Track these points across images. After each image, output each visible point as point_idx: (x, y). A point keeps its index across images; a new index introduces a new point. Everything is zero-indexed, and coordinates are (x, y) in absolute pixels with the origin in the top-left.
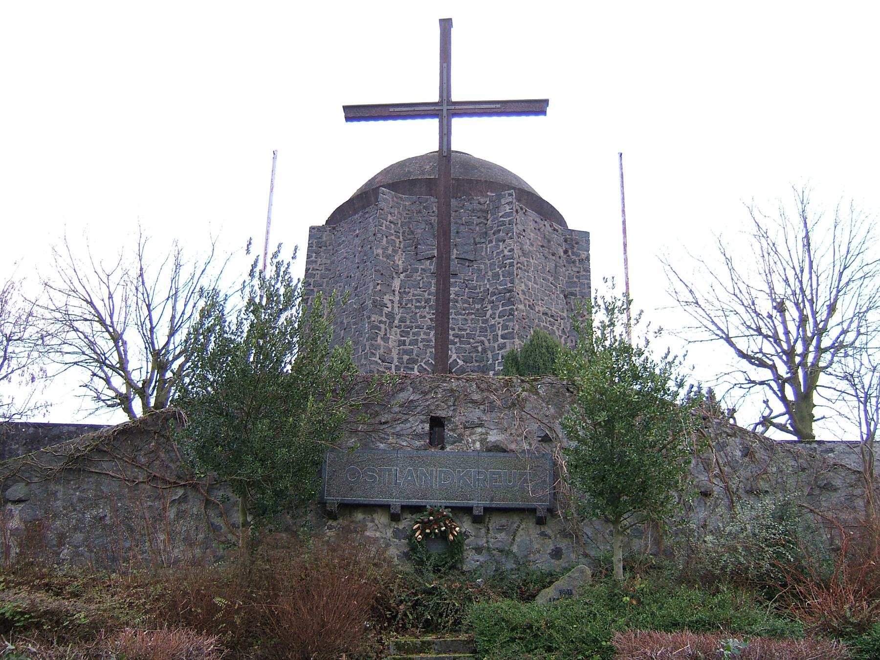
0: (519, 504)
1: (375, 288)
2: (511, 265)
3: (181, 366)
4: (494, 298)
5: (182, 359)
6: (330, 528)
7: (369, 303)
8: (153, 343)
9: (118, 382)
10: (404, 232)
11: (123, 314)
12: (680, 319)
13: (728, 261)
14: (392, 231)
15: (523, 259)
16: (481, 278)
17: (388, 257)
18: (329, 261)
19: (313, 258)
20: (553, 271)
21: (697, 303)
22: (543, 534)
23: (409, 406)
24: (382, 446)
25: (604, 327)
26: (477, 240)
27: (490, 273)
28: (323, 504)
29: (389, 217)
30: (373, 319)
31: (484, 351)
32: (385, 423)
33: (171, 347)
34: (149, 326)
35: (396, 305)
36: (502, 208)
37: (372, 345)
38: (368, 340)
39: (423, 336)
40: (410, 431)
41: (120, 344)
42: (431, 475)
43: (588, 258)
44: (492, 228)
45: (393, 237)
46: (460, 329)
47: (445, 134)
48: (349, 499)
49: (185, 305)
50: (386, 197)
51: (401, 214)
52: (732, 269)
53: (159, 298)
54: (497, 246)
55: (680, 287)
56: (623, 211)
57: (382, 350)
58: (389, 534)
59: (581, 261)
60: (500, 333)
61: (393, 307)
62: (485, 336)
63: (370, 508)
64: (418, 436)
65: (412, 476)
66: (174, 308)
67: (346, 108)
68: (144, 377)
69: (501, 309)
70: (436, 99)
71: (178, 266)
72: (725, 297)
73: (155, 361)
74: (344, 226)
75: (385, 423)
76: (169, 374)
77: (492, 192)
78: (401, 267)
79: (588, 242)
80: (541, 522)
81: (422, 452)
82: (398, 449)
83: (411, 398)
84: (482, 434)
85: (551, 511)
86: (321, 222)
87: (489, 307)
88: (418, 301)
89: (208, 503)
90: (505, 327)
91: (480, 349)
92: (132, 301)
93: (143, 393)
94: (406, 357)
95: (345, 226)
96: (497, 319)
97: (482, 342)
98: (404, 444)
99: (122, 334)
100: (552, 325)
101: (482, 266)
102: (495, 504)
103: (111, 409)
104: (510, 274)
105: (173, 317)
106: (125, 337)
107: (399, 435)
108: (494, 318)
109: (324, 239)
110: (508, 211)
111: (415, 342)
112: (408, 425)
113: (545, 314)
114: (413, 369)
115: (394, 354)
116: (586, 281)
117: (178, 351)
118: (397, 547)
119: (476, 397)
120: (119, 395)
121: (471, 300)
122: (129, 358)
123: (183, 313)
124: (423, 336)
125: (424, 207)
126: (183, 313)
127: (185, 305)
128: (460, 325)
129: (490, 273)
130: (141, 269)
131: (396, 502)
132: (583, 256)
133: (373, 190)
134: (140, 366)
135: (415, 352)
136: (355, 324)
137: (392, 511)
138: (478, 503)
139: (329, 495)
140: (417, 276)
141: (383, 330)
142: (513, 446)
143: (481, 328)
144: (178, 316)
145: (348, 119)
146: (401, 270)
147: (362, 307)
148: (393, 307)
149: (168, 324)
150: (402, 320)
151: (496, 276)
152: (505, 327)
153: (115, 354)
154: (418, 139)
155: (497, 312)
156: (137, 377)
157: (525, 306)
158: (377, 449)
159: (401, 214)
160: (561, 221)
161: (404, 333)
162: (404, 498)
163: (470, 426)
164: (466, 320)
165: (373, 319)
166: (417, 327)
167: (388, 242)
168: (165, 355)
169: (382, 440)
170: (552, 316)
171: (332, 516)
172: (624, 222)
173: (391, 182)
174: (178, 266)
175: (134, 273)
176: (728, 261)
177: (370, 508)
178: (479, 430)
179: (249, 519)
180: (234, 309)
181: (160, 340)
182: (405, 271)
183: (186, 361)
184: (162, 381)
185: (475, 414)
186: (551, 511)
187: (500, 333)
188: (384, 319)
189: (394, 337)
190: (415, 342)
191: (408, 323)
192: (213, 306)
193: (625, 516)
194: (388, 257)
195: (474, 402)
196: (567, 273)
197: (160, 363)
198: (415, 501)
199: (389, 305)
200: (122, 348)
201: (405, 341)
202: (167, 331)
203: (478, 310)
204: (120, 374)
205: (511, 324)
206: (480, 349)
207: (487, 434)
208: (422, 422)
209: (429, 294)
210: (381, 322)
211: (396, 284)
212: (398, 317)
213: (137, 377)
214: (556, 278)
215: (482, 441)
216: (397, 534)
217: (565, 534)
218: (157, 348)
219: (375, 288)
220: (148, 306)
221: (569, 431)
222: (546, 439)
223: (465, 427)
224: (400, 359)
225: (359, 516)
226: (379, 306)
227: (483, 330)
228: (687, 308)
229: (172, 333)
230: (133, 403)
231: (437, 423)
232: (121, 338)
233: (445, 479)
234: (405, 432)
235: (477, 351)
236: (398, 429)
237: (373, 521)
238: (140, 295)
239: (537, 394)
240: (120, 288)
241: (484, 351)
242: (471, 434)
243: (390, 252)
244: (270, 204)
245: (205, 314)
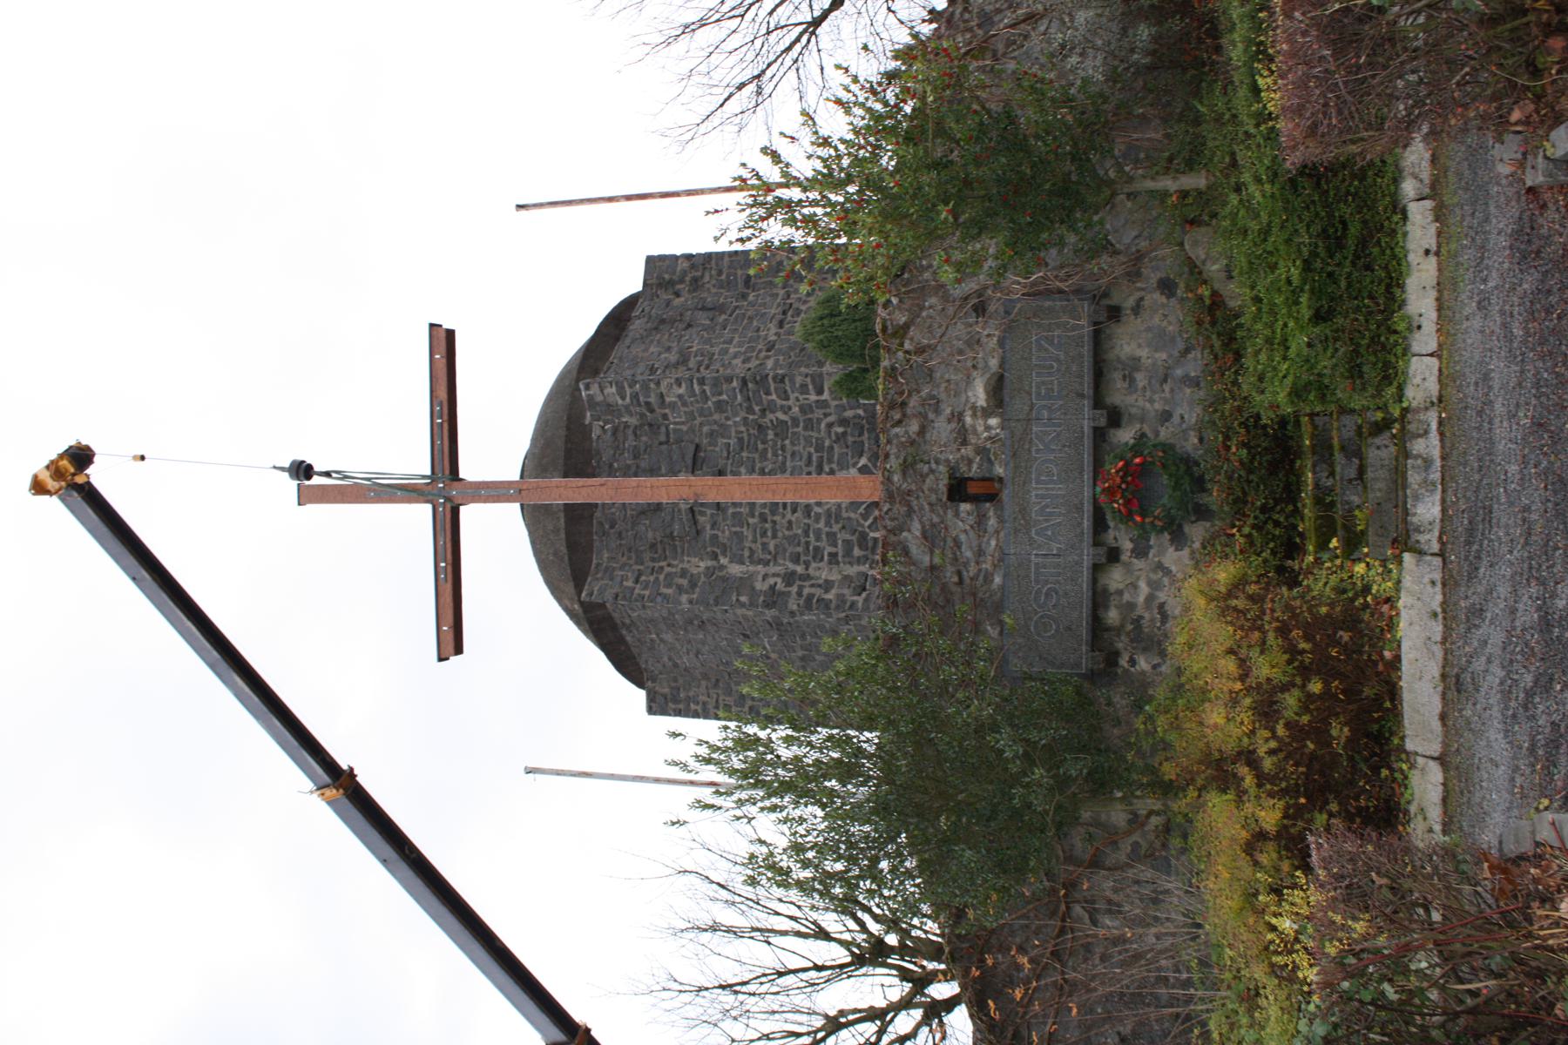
0: (1086, 350)
1: (743, 605)
2: (702, 382)
3: (876, 918)
4: (757, 409)
5: (866, 918)
6: (1133, 662)
7: (770, 614)
8: (842, 966)
9: (904, 1022)
10: (653, 560)
11: (798, 1017)
12: (783, 110)
13: (688, 29)
14: (652, 578)
15: (692, 364)
16: (723, 430)
17: (693, 585)
18: (704, 683)
19: (699, 708)
20: (710, 314)
21: (758, 77)
22: (1137, 309)
23: (931, 537)
24: (998, 580)
25: (791, 222)
26: (663, 438)
27: (716, 417)
28: (1092, 676)
29: (629, 584)
30: (795, 607)
31: (843, 422)
32: (959, 573)
33: (847, 937)
34: (813, 974)
35: (772, 569)
36: (610, 400)
37: (838, 607)
38: (829, 615)
39: (821, 525)
40: (972, 534)
41: (843, 1020)
42: (1043, 497)
43: (689, 257)
44: (642, 415)
45: (662, 577)
46: (809, 463)
47: (492, 492)
48: (1084, 632)
49: (777, 913)
50: (596, 589)
51: (624, 565)
52: (703, 23)
53: (762, 956)
54: (673, 406)
55: (733, 106)
56: (610, 199)
57: (846, 591)
58: (1138, 564)
59: (693, 267)
60: (813, 397)
61: (774, 575)
62: (819, 421)
63: (1099, 598)
64: (981, 520)
65: (1046, 529)
66: (784, 933)
67: (441, 659)
68: (896, 981)
69: (774, 397)
70: (427, 509)
71: (714, 928)
72: (747, 28)
73: (875, 963)
74: (646, 661)
75: (959, 573)
76: (892, 940)
77: (584, 417)
78: (710, 563)
79: (662, 258)
80: (1115, 313)
81: (1007, 513)
82: (1003, 556)
83: (918, 533)
84: (974, 415)
85: (1098, 297)
86: (641, 694)
87: (771, 416)
88: (764, 534)
89: (1095, 863)
90: (804, 389)
91: (840, 430)
92: (772, 1003)
93: (921, 982)
94: (857, 552)
95: (644, 656)
96: (790, 403)
97: (830, 425)
98: (993, 543)
99: (826, 1016)
100: (798, 312)
101: (705, 429)
102: (1087, 389)
103: (949, 1031)
104: (716, 383)
105: (798, 934)
106: (832, 1013)
107: (980, 553)
108: (790, 408)
109: (666, 690)
110: (614, 390)
111: (832, 538)
112: (963, 537)
113: (781, 324)
114: (875, 540)
115: (852, 570)
116: (726, 259)
117: (852, 925)
118: (1162, 552)
119: (914, 427)
120: (926, 1020)
121: (760, 446)
122: (865, 1006)
123: (791, 918)
124: (821, 525)
125: (612, 527)
126: (791, 918)
127: (777, 913)
128: (802, 463)
129: (716, 417)
130: (722, 987)
131: (1087, 556)
132: (686, 265)
133: (585, 612)
134: (878, 987)
135: (848, 537)
136: (803, 636)
137: (1104, 560)
138: (1087, 419)
139: (1078, 665)
140: (724, 536)
141: (813, 590)
142: (994, 363)
143: (805, 428)
144: (798, 927)
145: (459, 650)
146: (714, 563)
147: (776, 625)
148: (774, 575)
149: (810, 941)
150: (796, 559)
151: (720, 406)
152: (804, 389)
153: (860, 1027)
154: (498, 540)
155: (779, 402)
156: (898, 990)
157: (768, 357)
158: (1002, 587)
159: (624, 565)
160: (629, 304)
161: (817, 554)
162: (1081, 541)
163: (962, 436)
164: (793, 454)
165: (795, 607)
166: (806, 533)
167: (669, 586)
168: (859, 946)
169: (988, 578)
170: (784, 313)
171: (1112, 658)
172: (629, 198)
173: (572, 584)
174: (714, 928)
175: (728, 999)
176: (688, 29)
177: (1099, 598)
178: (968, 420)
179: (1119, 795)
180: (772, 831)
181: (841, 955)
182: (715, 557)
183: (868, 910)
184: (902, 950)
185: (942, 429)
186: (1098, 297)
187: (813, 397)
188: (794, 589)
189: (823, 572)
190: (832, 538)
191: (800, 549)
192: (765, 868)
193: (1101, 173)
194: (693, 585)
195: (922, 431)
196: (714, 290)
197: (871, 954)
198: (1087, 523)
199: (771, 581)
200: (851, 1017)
201: (830, 554)
202: (822, 944)
203: (776, 435)
204: (892, 1020)
205: (799, 380)
206: (840, 430)
207: (974, 408)
208: (957, 514)
209: (753, 516)
210: (800, 594)
211: (736, 570)
212: (791, 566)
213: (898, 990)
214: (721, 309)
215: (987, 413)
216: (1141, 551)
217: (1134, 274)
218: (849, 959)
219: (743, 605)
220: (780, 974)
221: (966, 264)
222: (980, 309)
223: (964, 443)
224: (859, 561)
225: (1113, 616)
226: (774, 598)
227: (809, 425)
228: (767, 91)
229: (822, 934)
230: (938, 997)
231: (958, 490)
232: (835, 1018)
233: (1050, 474)
234: (975, 543)
235: (844, 434)
236: (969, 554)
237: (1120, 593)
238: (763, 989)
239: (906, 327)
240: (752, 1022)
241: (843, 422)
242: (975, 432)
243: (685, 582)
244: (612, 777)
245: (782, 877)
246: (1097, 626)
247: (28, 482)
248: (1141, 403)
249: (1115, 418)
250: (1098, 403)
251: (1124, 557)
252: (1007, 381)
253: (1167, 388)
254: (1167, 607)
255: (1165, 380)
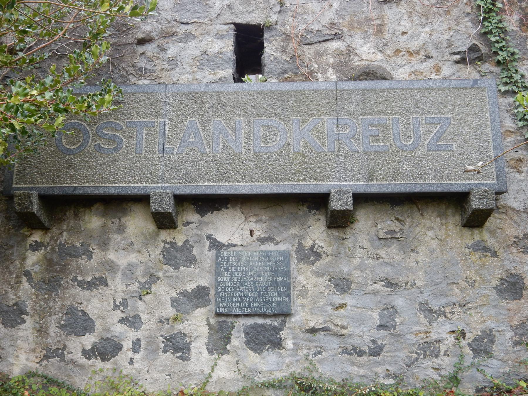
58: (157, 253)
63: (116, 203)
138: (340, 185)
139: (22, 178)
162: (181, 180)
177: (116, 203)
225: (93, 221)
246: (64, 205)
247: (252, 17)
248: (359, 253)
249: (339, 221)
250: (361, 199)
251: (165, 235)
252: (250, 236)
253: (379, 286)
254: (102, 289)
255: (390, 284)
